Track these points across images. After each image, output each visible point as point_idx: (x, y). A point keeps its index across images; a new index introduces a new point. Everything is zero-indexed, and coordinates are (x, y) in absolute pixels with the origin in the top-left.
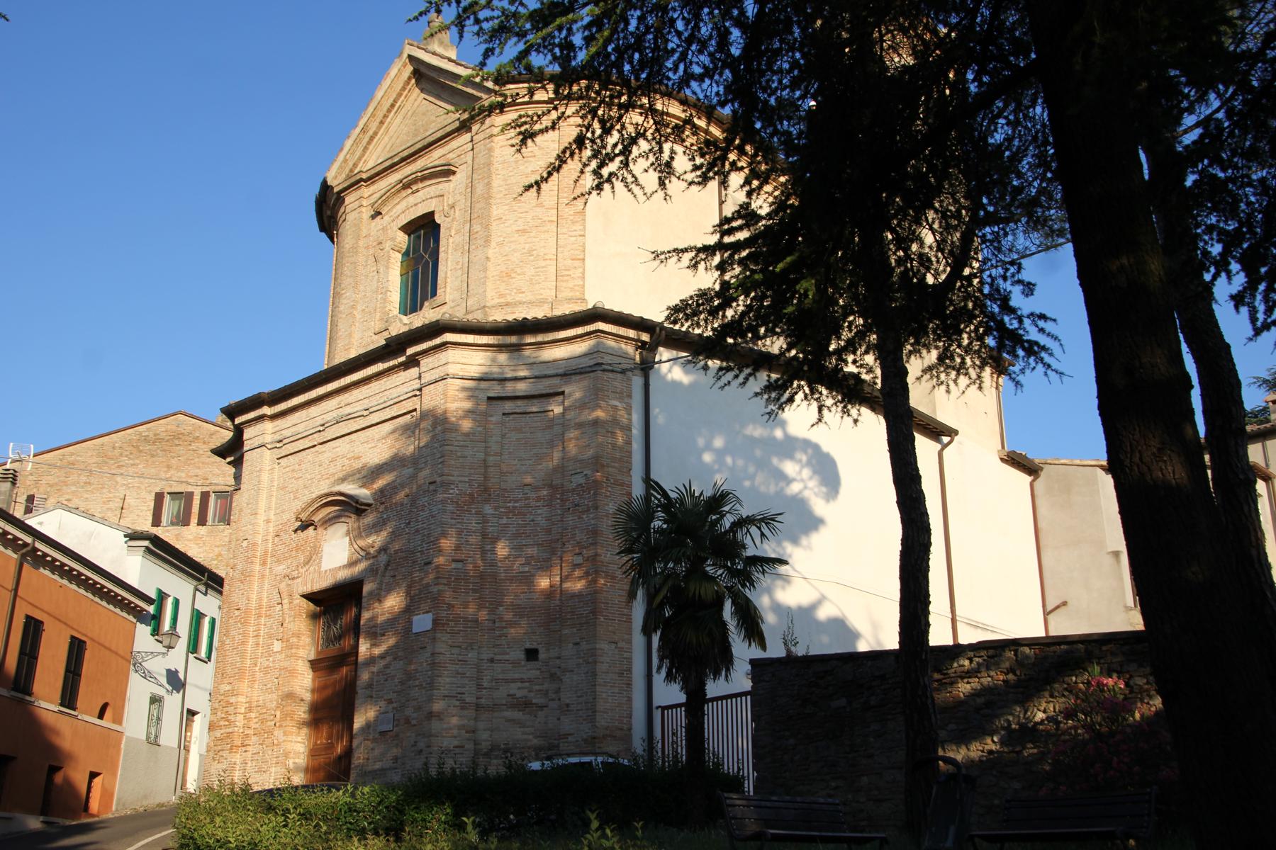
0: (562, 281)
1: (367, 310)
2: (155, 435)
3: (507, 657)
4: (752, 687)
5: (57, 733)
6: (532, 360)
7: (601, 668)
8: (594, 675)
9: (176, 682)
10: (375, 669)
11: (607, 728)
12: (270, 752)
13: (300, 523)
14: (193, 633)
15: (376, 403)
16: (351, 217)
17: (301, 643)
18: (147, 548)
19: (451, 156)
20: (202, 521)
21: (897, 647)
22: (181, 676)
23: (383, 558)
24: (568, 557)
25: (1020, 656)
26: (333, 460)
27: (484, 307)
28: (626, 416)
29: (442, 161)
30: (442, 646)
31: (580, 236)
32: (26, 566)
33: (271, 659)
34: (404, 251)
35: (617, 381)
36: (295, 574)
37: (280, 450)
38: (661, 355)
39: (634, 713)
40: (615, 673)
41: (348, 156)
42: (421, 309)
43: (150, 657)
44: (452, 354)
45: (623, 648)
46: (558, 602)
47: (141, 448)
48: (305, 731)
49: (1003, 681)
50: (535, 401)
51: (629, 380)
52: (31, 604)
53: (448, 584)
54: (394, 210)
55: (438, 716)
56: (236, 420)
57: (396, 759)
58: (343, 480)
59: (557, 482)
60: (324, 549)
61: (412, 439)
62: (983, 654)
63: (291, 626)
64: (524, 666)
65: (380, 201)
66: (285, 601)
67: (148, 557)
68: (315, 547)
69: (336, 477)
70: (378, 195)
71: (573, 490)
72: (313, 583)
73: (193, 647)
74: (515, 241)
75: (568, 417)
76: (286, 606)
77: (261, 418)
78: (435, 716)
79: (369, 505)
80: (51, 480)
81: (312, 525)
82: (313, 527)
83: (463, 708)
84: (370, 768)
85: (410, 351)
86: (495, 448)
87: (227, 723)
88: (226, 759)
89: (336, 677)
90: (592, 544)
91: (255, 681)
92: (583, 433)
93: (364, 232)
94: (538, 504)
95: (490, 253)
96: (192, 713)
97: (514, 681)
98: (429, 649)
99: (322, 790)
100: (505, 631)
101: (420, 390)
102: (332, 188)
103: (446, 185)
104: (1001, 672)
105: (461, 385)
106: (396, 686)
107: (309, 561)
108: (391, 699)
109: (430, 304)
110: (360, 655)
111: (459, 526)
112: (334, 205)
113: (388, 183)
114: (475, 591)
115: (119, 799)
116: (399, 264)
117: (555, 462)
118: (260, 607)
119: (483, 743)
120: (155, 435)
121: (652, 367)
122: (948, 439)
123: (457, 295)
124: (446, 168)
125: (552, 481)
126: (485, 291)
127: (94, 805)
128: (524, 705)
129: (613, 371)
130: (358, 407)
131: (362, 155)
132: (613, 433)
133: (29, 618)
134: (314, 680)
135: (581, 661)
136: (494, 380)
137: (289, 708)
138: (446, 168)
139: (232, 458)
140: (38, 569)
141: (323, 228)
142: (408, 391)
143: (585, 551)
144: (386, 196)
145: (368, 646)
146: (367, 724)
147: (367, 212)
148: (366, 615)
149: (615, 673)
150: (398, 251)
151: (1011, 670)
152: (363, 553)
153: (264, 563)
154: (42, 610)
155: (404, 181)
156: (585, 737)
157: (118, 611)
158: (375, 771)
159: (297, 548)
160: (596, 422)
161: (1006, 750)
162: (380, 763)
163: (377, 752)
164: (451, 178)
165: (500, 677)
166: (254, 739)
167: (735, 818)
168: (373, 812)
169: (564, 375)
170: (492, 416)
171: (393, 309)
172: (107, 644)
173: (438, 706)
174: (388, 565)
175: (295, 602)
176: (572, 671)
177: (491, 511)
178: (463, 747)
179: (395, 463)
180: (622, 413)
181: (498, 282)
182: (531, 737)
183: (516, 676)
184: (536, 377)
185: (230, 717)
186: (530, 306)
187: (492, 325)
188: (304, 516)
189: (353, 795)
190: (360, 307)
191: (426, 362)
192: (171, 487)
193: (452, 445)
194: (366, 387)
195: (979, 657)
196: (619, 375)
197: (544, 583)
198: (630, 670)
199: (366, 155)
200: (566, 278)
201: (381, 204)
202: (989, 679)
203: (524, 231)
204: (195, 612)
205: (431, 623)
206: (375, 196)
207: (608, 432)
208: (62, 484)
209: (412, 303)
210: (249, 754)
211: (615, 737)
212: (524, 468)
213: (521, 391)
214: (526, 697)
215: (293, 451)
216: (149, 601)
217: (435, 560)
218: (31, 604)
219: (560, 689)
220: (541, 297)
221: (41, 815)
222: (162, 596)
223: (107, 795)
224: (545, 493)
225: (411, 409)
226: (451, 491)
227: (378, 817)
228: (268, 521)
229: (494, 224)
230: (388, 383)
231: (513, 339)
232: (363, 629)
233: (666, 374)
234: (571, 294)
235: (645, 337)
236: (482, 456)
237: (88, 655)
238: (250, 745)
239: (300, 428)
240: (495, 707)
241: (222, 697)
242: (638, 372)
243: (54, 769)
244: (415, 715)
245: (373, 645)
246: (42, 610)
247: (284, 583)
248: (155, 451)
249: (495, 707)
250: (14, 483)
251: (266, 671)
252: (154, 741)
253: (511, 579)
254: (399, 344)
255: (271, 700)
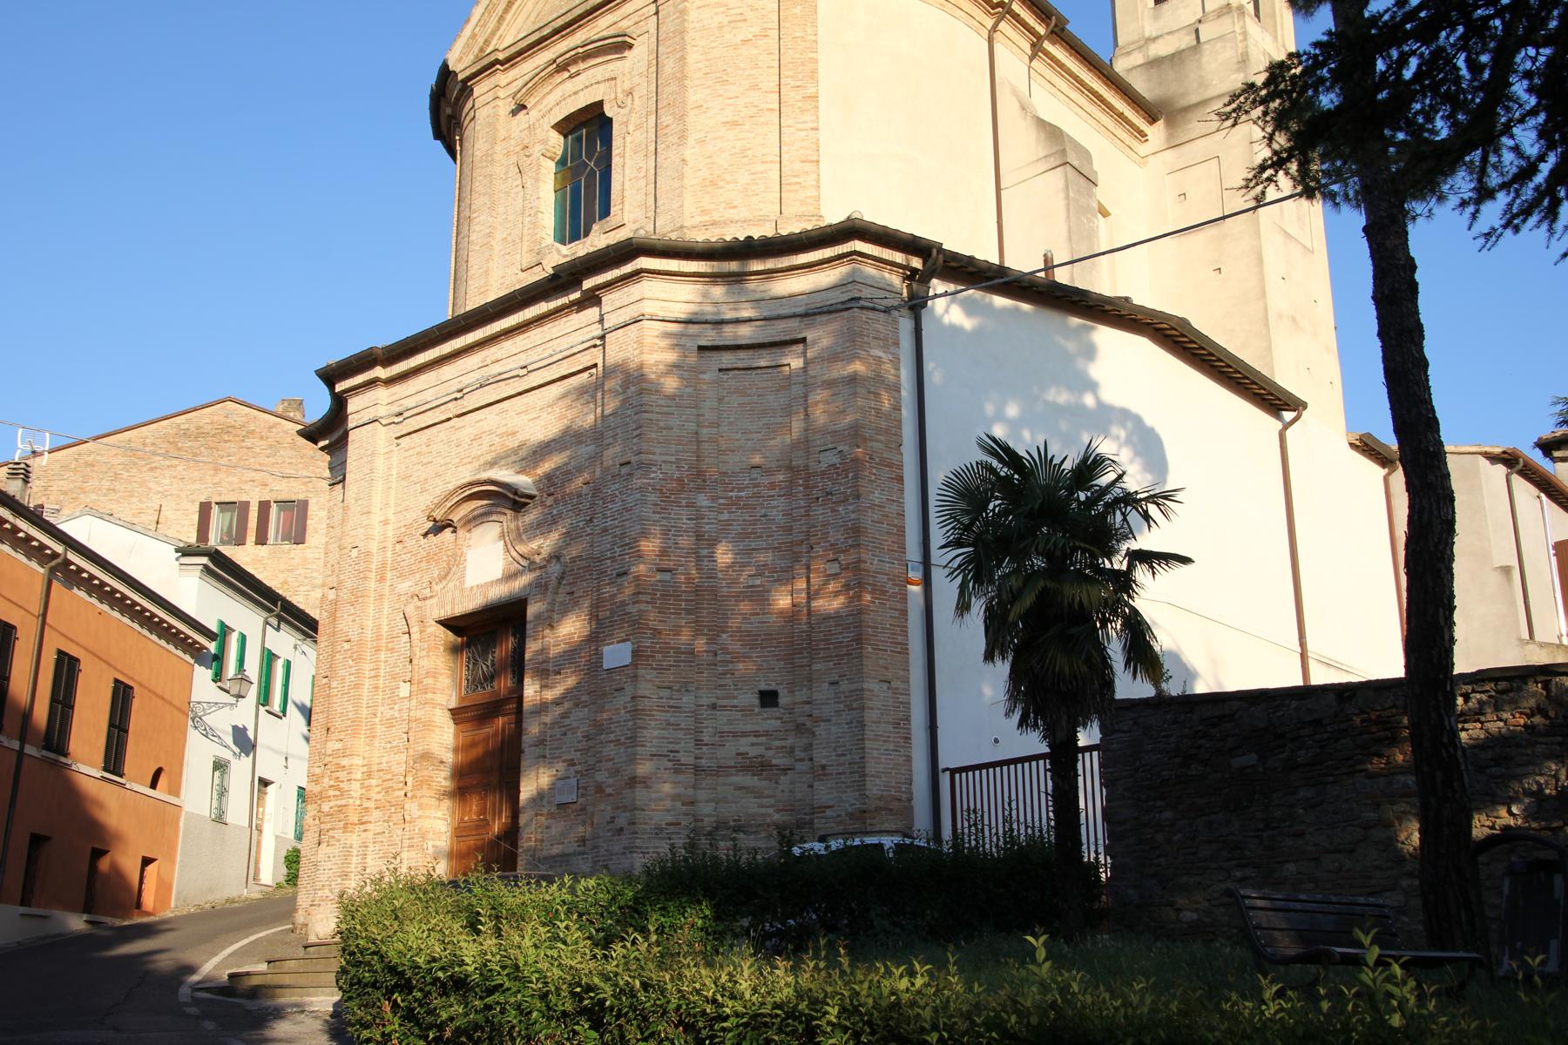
0: (789, 191)
1: (509, 239)
2: (198, 428)
3: (735, 702)
4: (1101, 740)
5: (101, 805)
6: (758, 296)
7: (870, 716)
8: (862, 725)
9: (244, 742)
10: (547, 719)
11: (881, 798)
12: (400, 832)
13: (431, 524)
14: (263, 679)
15: (537, 358)
16: (482, 114)
17: (439, 685)
18: (205, 566)
19: (624, 24)
20: (261, 540)
21: (1403, 675)
22: (251, 734)
23: (555, 568)
24: (819, 565)
25: (1553, 689)
26: (477, 437)
27: (682, 227)
28: (893, 371)
29: (611, 32)
30: (648, 687)
31: (812, 129)
32: (55, 584)
33: (396, 707)
34: (558, 158)
35: (879, 323)
36: (427, 592)
37: (400, 426)
38: (934, 290)
39: (915, 778)
40: (888, 723)
41: (477, 29)
42: (587, 234)
43: (214, 709)
44: (647, 287)
45: (897, 689)
46: (805, 627)
47: (180, 445)
48: (447, 803)
49: (1525, 726)
50: (764, 352)
51: (895, 322)
52: (62, 634)
53: (652, 602)
54: (545, 102)
55: (645, 782)
56: (337, 386)
57: (583, 841)
58: (492, 464)
59: (798, 462)
60: (468, 557)
61: (592, 406)
62: (1487, 688)
63: (424, 662)
64: (759, 714)
65: (524, 90)
66: (414, 630)
67: (204, 577)
68: (454, 555)
69: (482, 460)
70: (520, 82)
71: (823, 473)
72: (453, 604)
73: (265, 699)
74: (721, 138)
75: (811, 373)
76: (415, 636)
77: (372, 383)
78: (640, 782)
79: (532, 497)
80: (65, 485)
81: (450, 525)
82: (451, 529)
83: (677, 771)
84: (545, 853)
85: (588, 284)
86: (710, 416)
87: (338, 793)
88: (339, 840)
89: (488, 730)
90: (852, 546)
91: (374, 737)
92: (833, 395)
93: (502, 134)
94: (772, 493)
95: (688, 153)
96: (264, 783)
97: (744, 734)
98: (629, 691)
99: (528, 884)
100: (731, 666)
101: (603, 337)
102: (456, 74)
103: (619, 63)
104: (1521, 713)
105: (661, 329)
106: (578, 742)
107: (447, 575)
108: (572, 760)
109: (601, 227)
110: (525, 700)
111: (664, 522)
112: (457, 99)
113: (534, 65)
114: (688, 612)
115: (178, 893)
116: (553, 176)
117: (795, 435)
118: (378, 638)
119: (706, 819)
120: (198, 428)
121: (924, 305)
122: (1293, 414)
123: (640, 213)
124: (619, 39)
125: (791, 462)
126: (682, 206)
127: (149, 900)
128: (761, 767)
129: (874, 309)
130: (512, 364)
131: (498, 28)
132: (877, 395)
133: (61, 654)
134: (456, 736)
135: (841, 706)
136: (706, 322)
137: (425, 773)
138: (619, 39)
139: (327, 442)
140: (70, 588)
141: (438, 134)
142: (584, 339)
143: (842, 557)
144: (533, 82)
145: (537, 687)
146: (539, 793)
147: (506, 106)
148: (532, 647)
149: (888, 723)
150: (550, 158)
151: (1539, 710)
152: (524, 563)
153: (382, 579)
154: (77, 644)
155: (558, 61)
156: (850, 810)
157: (171, 647)
158: (553, 857)
159: (429, 558)
160: (853, 379)
161: (1534, 825)
162: (560, 847)
163: (554, 831)
164: (626, 53)
165: (726, 729)
166: (376, 814)
167: (1259, 927)
168: (602, 915)
169: (806, 315)
170: (704, 373)
171: (546, 237)
172: (159, 691)
173: (643, 769)
174: (562, 578)
175: (428, 630)
176: (829, 721)
177: (706, 503)
178: (679, 824)
179: (567, 439)
180: (888, 366)
181: (700, 194)
182: (771, 811)
183: (749, 728)
184: (765, 319)
185: (342, 785)
186: (745, 225)
187: (705, 245)
188: (438, 514)
189: (572, 891)
190: (499, 235)
191: (610, 300)
192: (220, 495)
193: (652, 412)
194: (521, 337)
195: (1480, 692)
196: (882, 315)
197: (783, 601)
198: (907, 719)
199: (502, 28)
200: (793, 187)
201: (526, 94)
202: (1501, 724)
203: (735, 124)
204: (266, 652)
205: (630, 654)
206: (515, 83)
207: (869, 392)
208: (79, 491)
209: (573, 225)
210: (370, 835)
211: (891, 810)
212: (750, 443)
213: (744, 337)
214: (762, 756)
215: (418, 428)
216: (211, 635)
217: (633, 569)
218: (62, 634)
219: (811, 745)
220: (761, 213)
221: (84, 912)
222: (225, 630)
223: (164, 887)
224: (781, 477)
225: (589, 364)
226: (653, 475)
227: (609, 922)
228: (386, 522)
229: (691, 114)
230: (554, 330)
231: (733, 266)
232: (528, 666)
233: (943, 315)
234: (801, 210)
235: (916, 263)
236: (692, 427)
237: (136, 705)
238: (370, 822)
239: (429, 395)
240: (720, 770)
241: (330, 759)
242: (905, 312)
243: (99, 853)
244: (611, 781)
245: (543, 687)
246: (77, 644)
247: (412, 606)
248: (198, 448)
249: (720, 770)
250: (26, 481)
251: (390, 723)
252: (220, 819)
253: (739, 597)
254: (572, 274)
255: (398, 762)
